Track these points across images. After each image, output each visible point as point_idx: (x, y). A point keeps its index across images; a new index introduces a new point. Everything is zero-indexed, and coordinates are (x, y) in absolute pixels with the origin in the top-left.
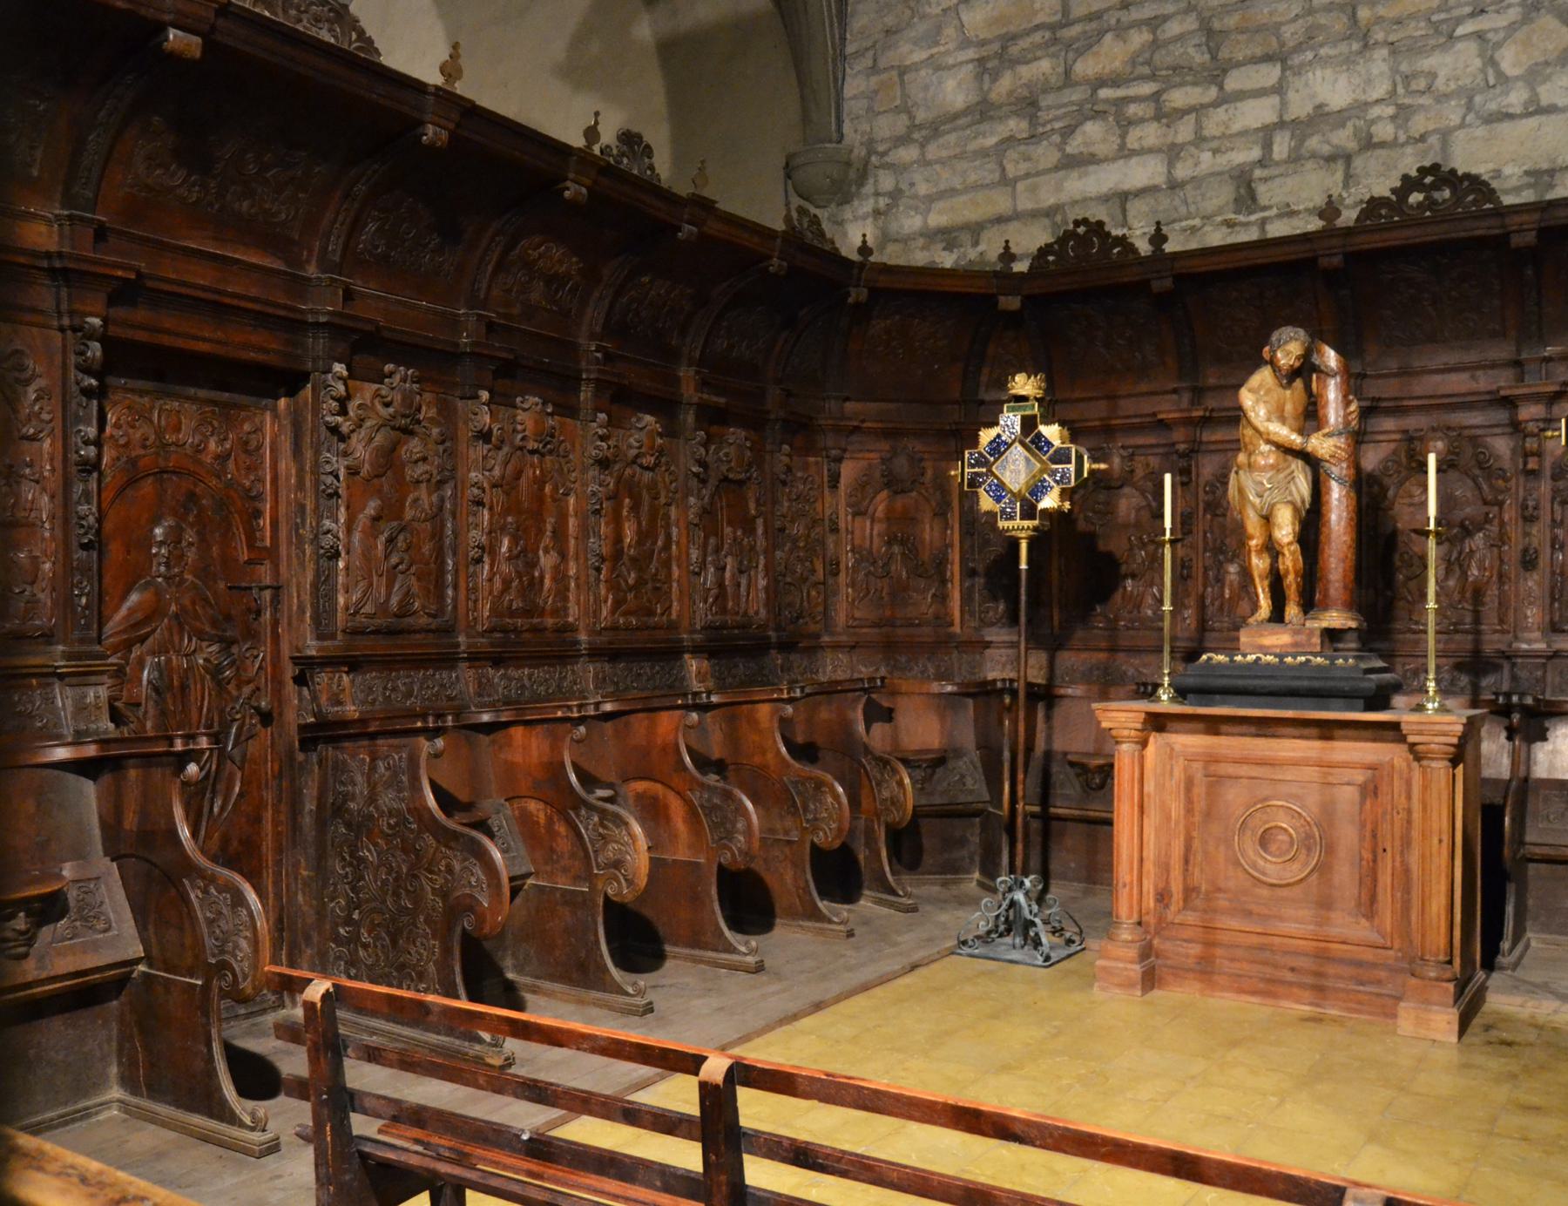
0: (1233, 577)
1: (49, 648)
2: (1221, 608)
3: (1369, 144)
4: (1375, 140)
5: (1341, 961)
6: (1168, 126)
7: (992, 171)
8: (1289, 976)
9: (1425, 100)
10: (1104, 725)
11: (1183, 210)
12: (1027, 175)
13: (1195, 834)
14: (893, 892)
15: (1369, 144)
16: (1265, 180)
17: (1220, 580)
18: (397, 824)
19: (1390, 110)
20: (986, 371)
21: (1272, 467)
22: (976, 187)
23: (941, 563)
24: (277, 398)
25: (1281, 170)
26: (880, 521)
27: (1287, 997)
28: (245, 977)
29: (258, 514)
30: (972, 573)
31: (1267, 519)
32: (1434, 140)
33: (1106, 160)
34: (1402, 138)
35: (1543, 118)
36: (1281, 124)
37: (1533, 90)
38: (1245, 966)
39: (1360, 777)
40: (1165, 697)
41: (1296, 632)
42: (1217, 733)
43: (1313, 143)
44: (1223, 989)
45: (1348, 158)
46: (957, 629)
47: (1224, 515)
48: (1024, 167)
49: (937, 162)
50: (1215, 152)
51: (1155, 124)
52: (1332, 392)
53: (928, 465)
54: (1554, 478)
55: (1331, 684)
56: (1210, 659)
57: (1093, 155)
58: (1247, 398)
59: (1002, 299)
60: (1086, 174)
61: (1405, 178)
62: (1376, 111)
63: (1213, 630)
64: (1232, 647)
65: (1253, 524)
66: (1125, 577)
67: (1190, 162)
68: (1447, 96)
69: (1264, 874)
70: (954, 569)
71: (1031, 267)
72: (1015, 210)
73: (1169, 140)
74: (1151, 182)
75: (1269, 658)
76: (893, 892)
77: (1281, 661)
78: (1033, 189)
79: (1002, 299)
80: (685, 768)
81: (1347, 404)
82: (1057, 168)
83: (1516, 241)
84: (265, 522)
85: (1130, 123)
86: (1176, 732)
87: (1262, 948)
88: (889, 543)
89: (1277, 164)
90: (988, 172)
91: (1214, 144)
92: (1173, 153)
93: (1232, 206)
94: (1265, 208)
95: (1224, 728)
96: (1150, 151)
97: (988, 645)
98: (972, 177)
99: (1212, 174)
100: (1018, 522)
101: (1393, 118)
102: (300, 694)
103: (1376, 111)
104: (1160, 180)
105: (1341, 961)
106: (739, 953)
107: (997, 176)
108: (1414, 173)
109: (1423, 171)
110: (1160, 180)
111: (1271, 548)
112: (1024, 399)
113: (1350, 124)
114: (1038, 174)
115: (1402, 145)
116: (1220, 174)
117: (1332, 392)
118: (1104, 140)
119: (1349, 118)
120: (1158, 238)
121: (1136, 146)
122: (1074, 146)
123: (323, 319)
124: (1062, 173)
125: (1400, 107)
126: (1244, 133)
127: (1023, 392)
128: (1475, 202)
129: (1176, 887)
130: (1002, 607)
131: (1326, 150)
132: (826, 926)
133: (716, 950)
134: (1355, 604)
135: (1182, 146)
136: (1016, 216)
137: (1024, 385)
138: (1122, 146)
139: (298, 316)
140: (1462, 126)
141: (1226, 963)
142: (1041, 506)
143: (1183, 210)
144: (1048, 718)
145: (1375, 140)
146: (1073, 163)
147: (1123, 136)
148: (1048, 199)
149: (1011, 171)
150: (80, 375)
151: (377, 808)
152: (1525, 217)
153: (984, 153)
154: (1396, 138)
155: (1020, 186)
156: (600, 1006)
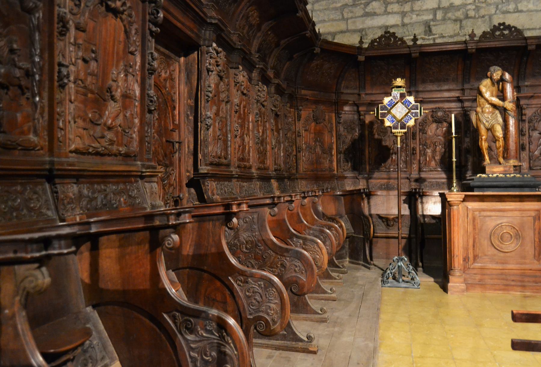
1: (134, 163)
2: (426, 164)
3: (467, 17)
4: (469, 16)
5: (529, 276)
6: (402, 5)
7: (338, 15)
8: (513, 283)
9: (484, 5)
10: (448, 200)
11: (407, 33)
12: (352, 18)
13: (476, 237)
14: (339, 267)
15: (467, 17)
16: (434, 25)
17: (425, 155)
18: (252, 247)
19: (474, 7)
20: (343, 82)
21: (491, 112)
22: (333, 20)
23: (331, 149)
24: (180, 57)
25: (440, 22)
26: (312, 133)
27: (512, 290)
28: (274, 322)
29: (174, 108)
30: (340, 153)
32: (487, 17)
33: (380, 15)
34: (477, 16)
35: (520, 14)
36: (439, 8)
37: (516, 5)
38: (496, 281)
39: (533, 214)
40: (455, 190)
41: (504, 167)
42: (483, 201)
43: (449, 15)
44: (490, 289)
45: (461, 21)
46: (335, 172)
47: (426, 133)
48: (350, 15)
49: (318, 10)
50: (417, 15)
51: (397, 5)
52: (509, 88)
53: (326, 114)
54: (529, 123)
55: (526, 183)
56: (480, 176)
57: (375, 13)
59: (359, 56)
60: (373, 19)
61: (494, 26)
62: (469, 7)
63: (423, 171)
66: (392, 154)
67: (409, 17)
68: (490, 4)
69: (502, 248)
70: (334, 152)
71: (368, 46)
72: (347, 29)
73: (402, 10)
74: (396, 23)
75: (501, 175)
76: (339, 267)
77: (506, 176)
78: (354, 22)
79: (359, 56)
80: (317, 220)
81: (513, 93)
82: (362, 16)
83: (530, 48)
84: (177, 112)
85: (389, 3)
86: (469, 201)
87: (502, 274)
88: (315, 142)
89: (438, 21)
90: (338, 16)
91: (417, 13)
92: (404, 14)
93: (423, 33)
94: (434, 35)
95: (506, 199)
96: (395, 13)
97: (346, 178)
98: (332, 17)
99: (416, 22)
100: (399, 130)
101: (474, 10)
102: (189, 191)
103: (469, 7)
104: (399, 23)
105: (529, 276)
106: (329, 293)
107: (341, 17)
108: (497, 25)
109: (500, 24)
110: (399, 23)
112: (400, 87)
113: (461, 10)
114: (356, 17)
115: (477, 18)
116: (419, 22)
117: (509, 88)
118: (380, 8)
119: (461, 8)
120: (415, 39)
121: (391, 11)
122: (369, 9)
123: (213, 22)
124: (364, 18)
125: (477, 6)
126: (427, 10)
127: (400, 85)
128: (516, 35)
129: (471, 256)
130: (349, 164)
131: (454, 18)
132: (333, 281)
133: (317, 293)
135: (406, 12)
136: (347, 31)
137: (399, 82)
138: (386, 11)
139: (204, 17)
140: (495, 14)
141: (489, 280)
142: (408, 124)
143: (407, 33)
144: (369, 203)
145: (469, 16)
146: (367, 15)
147: (386, 7)
148: (360, 26)
149: (346, 16)
150: (151, 26)
151: (239, 241)
152: (533, 41)
153: (336, 9)
154: (475, 16)
155: (349, 21)
156: (306, 320)
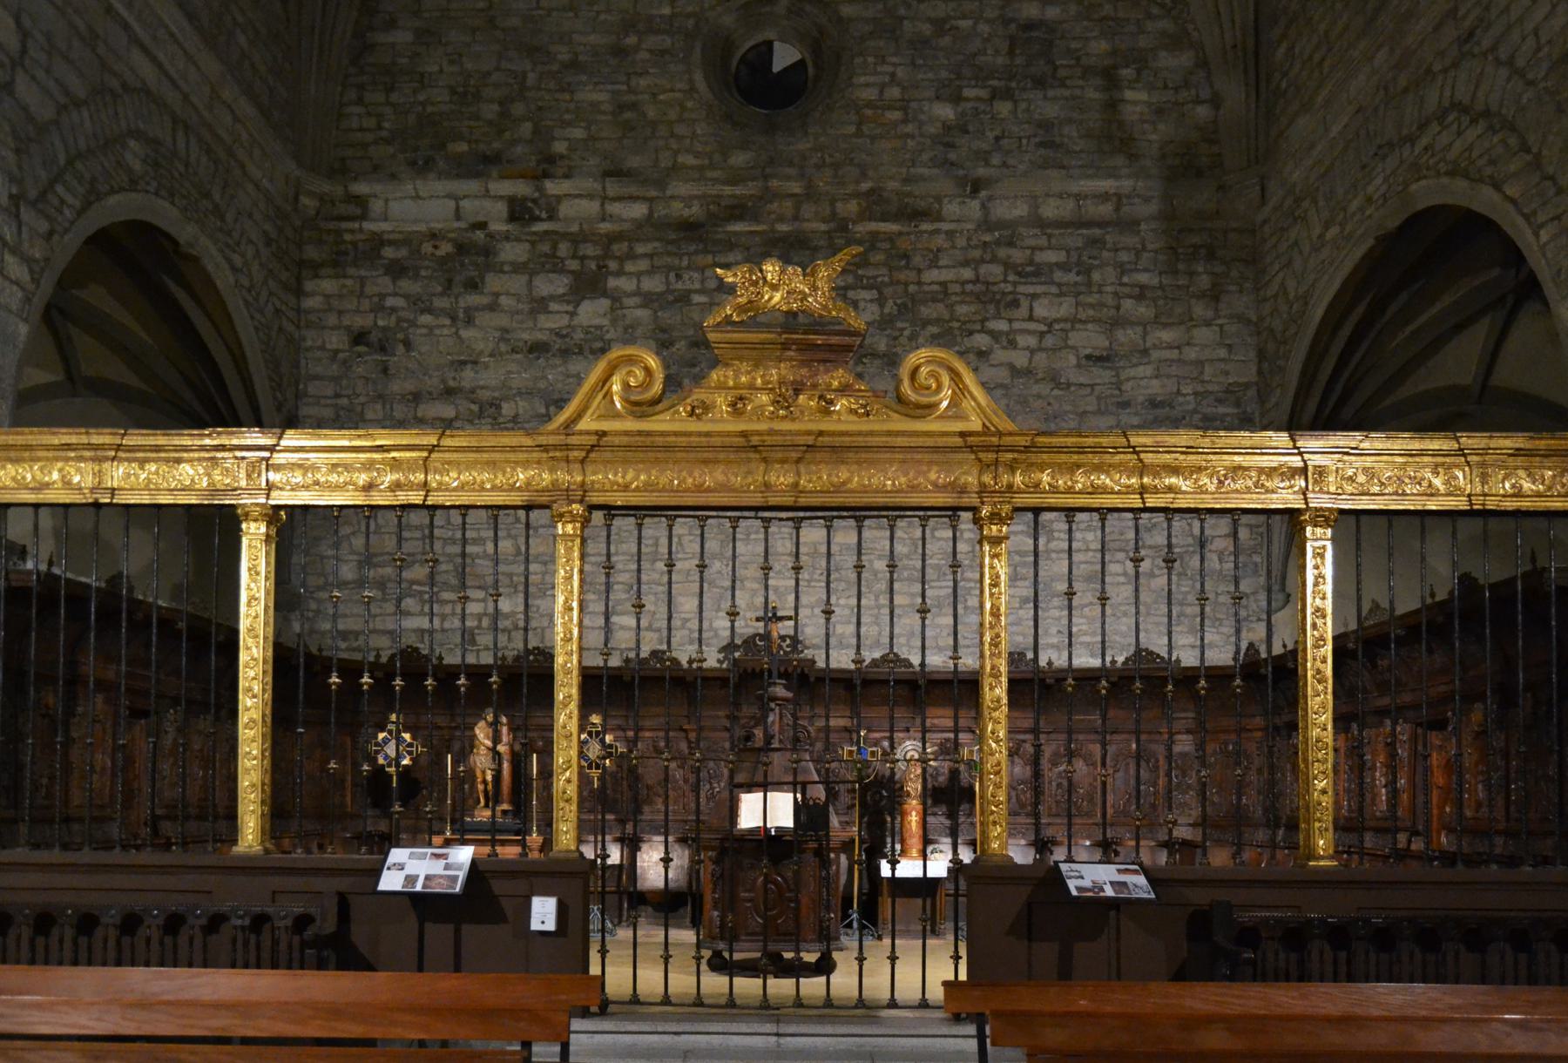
0: (1058, 11)
31: (484, 772)
52: (505, 730)
58: (477, 731)
64: (472, 816)
65: (479, 774)
111: (485, 782)
134: (511, 802)
